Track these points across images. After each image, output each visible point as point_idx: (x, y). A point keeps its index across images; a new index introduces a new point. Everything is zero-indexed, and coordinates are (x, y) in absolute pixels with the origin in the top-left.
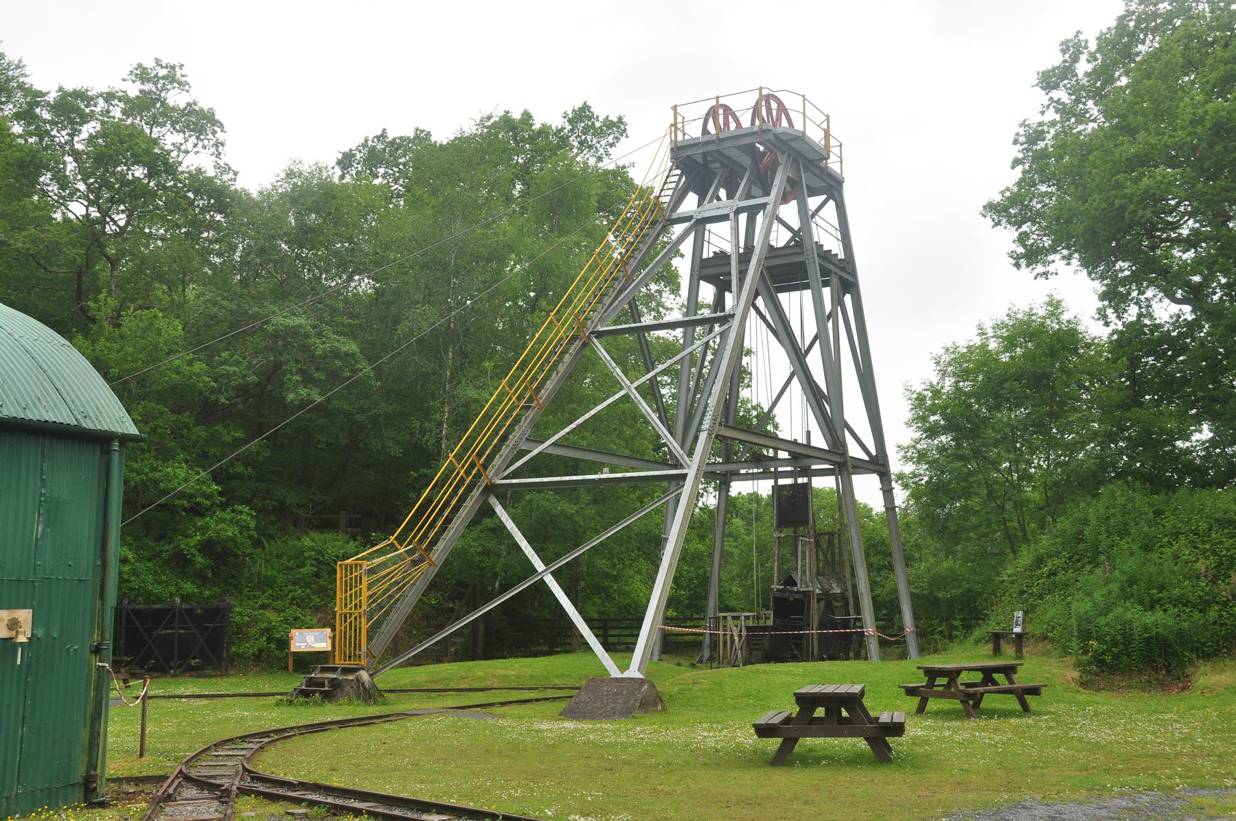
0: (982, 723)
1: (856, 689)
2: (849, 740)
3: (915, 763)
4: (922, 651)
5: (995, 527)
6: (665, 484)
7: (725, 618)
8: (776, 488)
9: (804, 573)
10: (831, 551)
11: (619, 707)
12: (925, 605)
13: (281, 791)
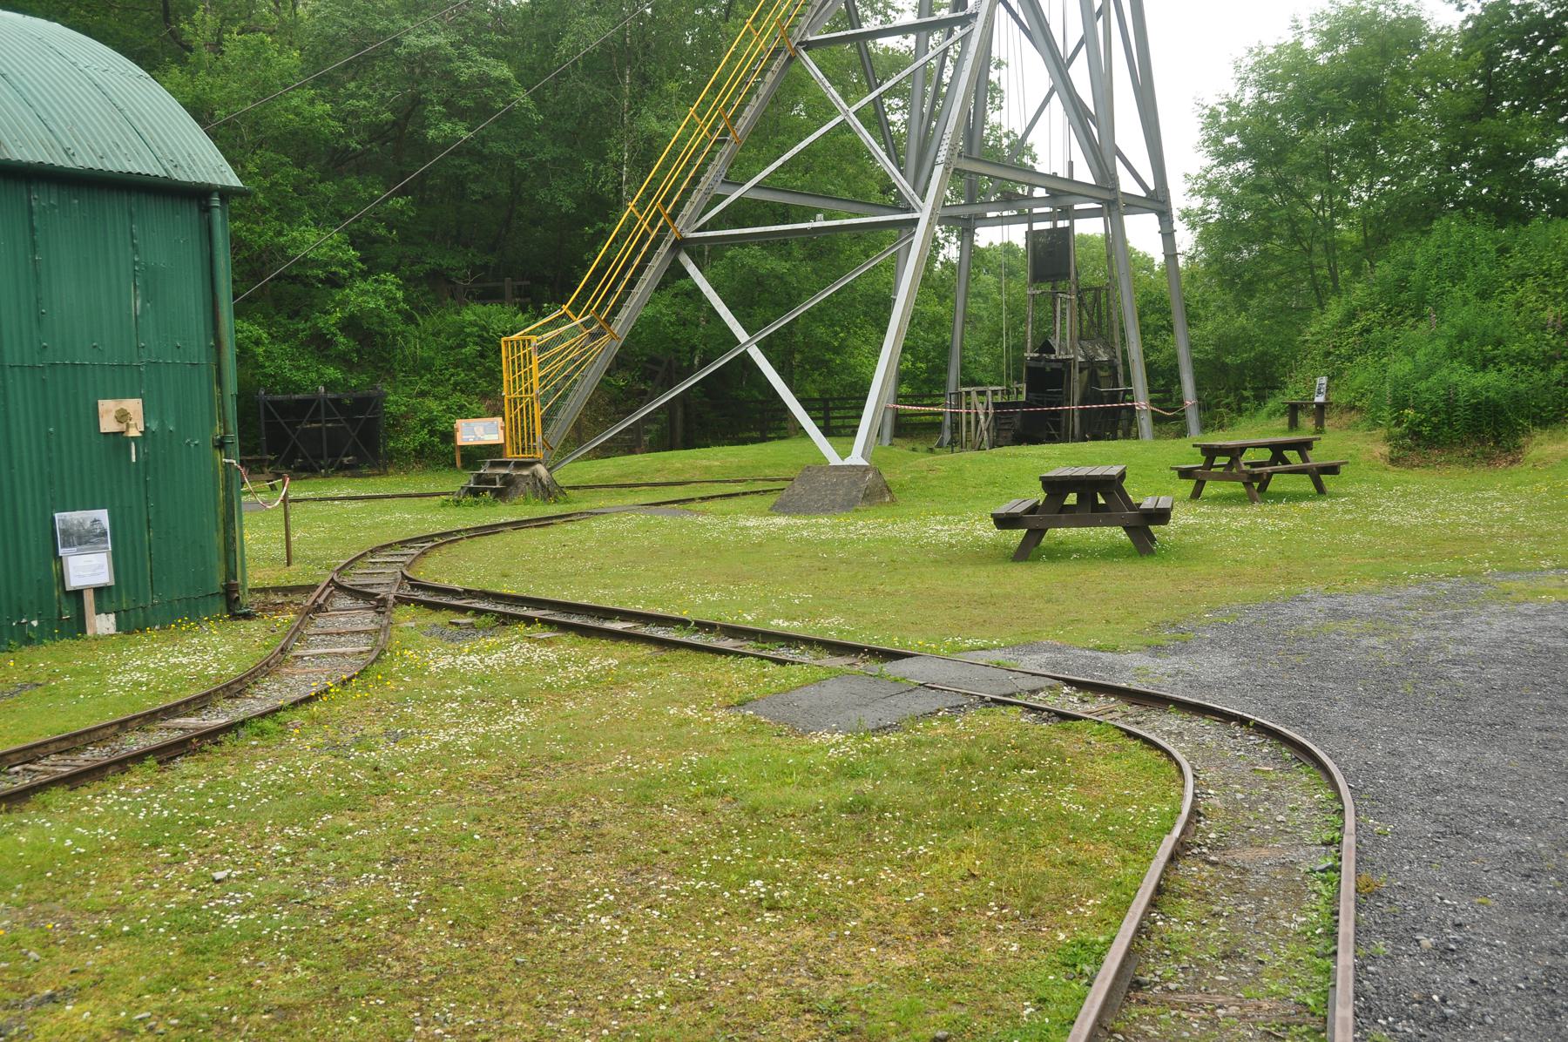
0: (1267, 508)
1: (1115, 471)
2: (1107, 530)
3: (1182, 554)
4: (1204, 427)
5: (1300, 275)
6: (895, 232)
7: (968, 393)
8: (1032, 236)
9: (1063, 339)
10: (1096, 311)
12: (1212, 373)
13: (444, 600)
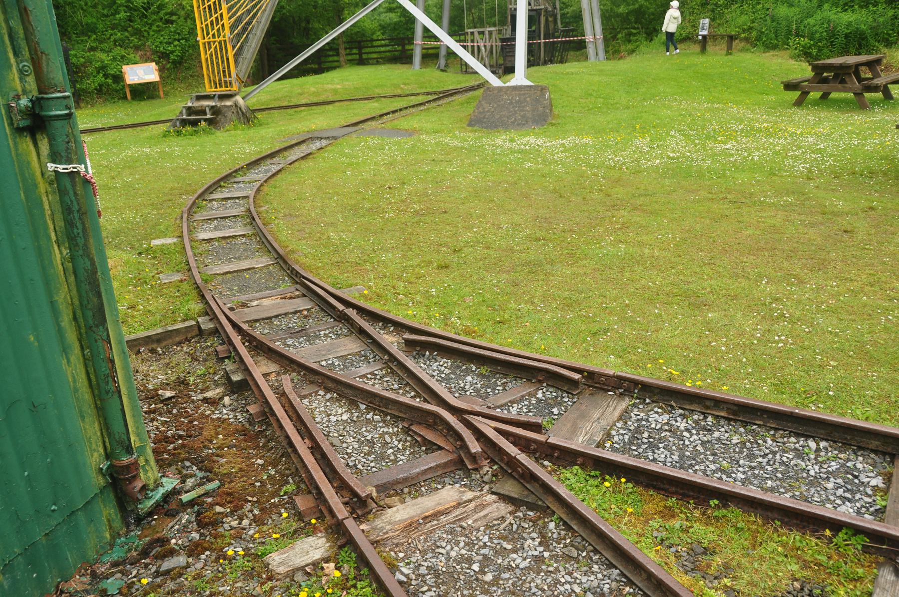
7: (472, 33)
11: (529, 115)
